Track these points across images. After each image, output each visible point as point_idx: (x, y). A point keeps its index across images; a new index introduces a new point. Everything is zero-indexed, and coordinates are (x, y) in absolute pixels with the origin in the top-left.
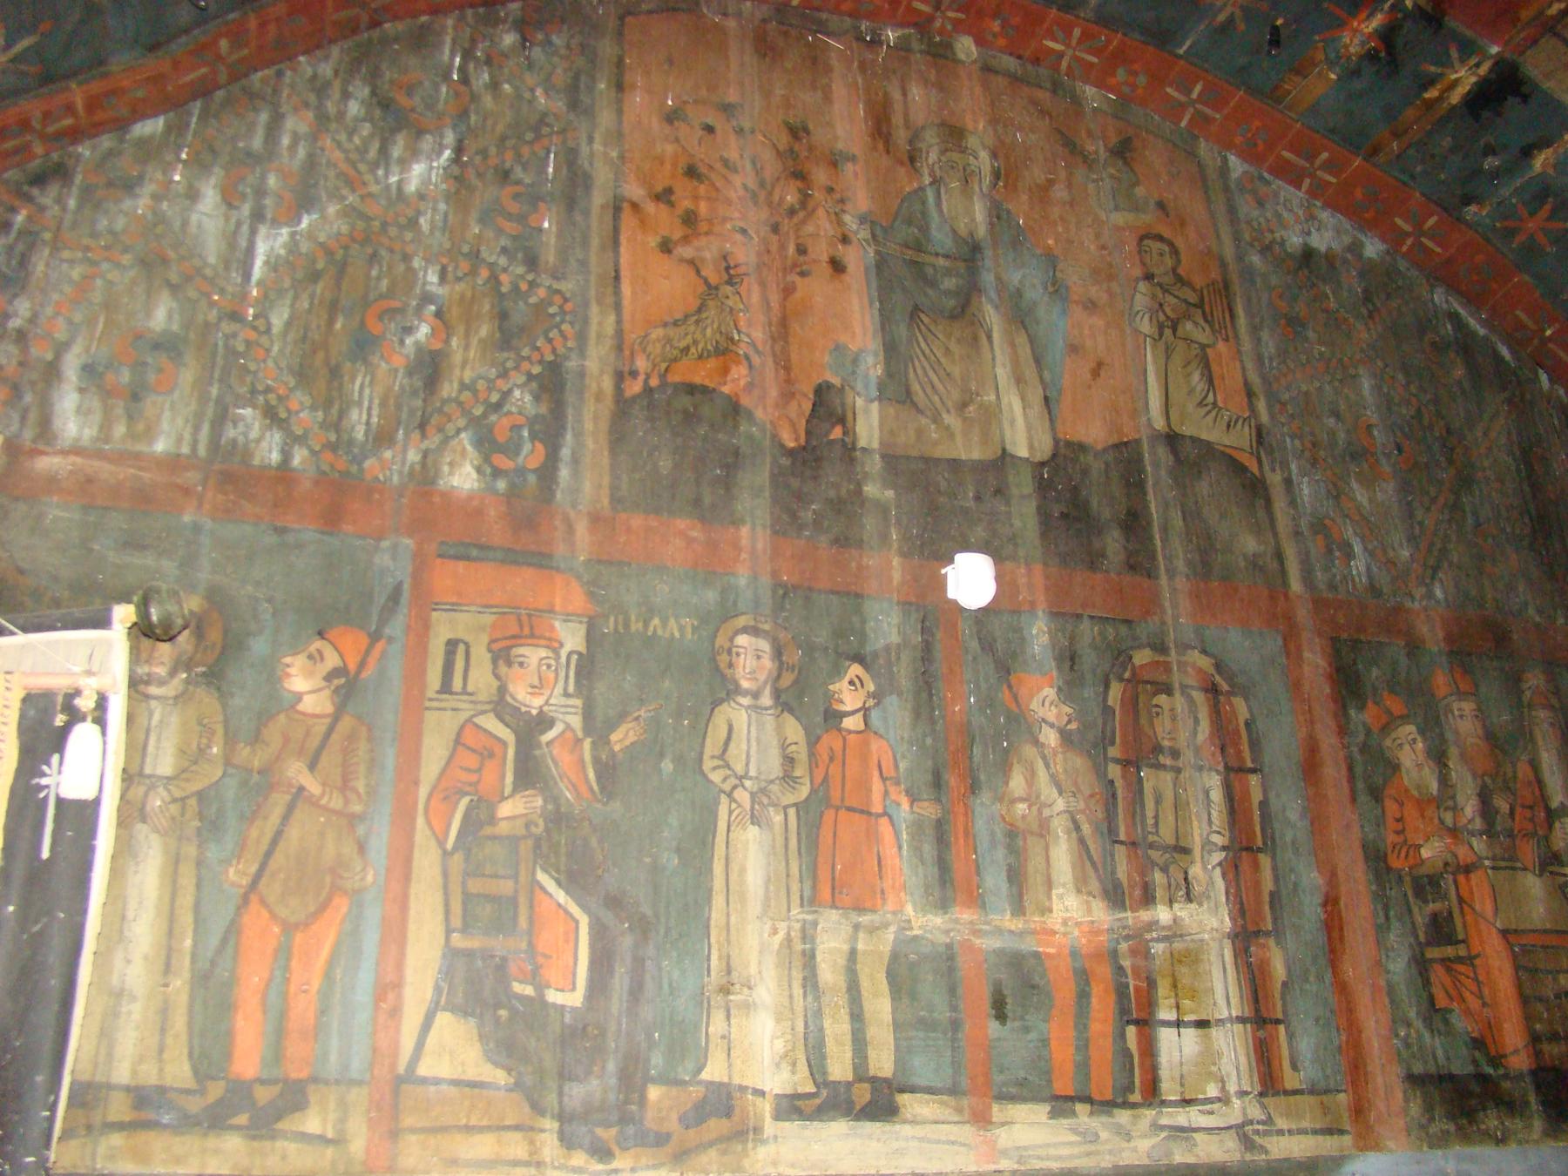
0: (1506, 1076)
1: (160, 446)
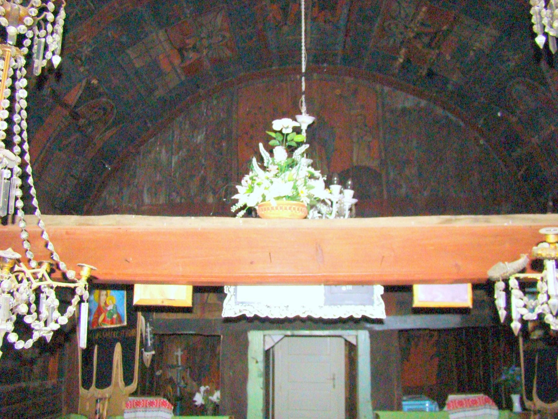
0: (19, 102)
1: (161, 202)
